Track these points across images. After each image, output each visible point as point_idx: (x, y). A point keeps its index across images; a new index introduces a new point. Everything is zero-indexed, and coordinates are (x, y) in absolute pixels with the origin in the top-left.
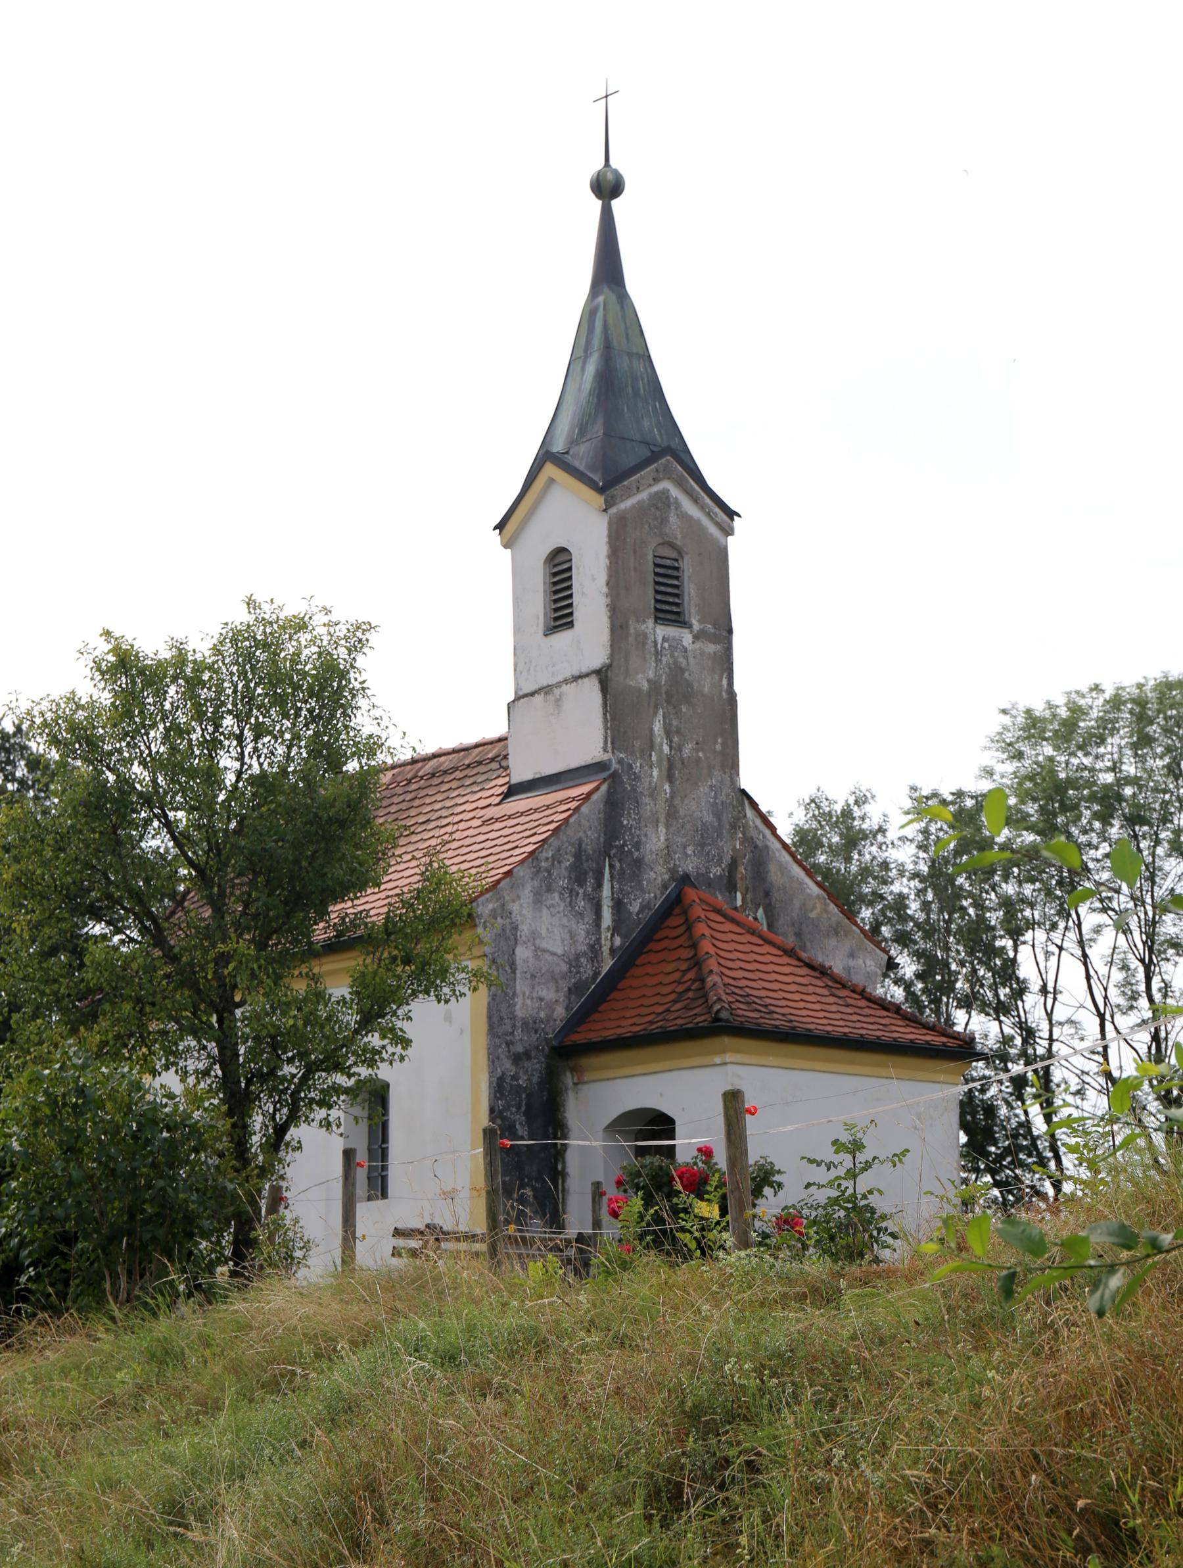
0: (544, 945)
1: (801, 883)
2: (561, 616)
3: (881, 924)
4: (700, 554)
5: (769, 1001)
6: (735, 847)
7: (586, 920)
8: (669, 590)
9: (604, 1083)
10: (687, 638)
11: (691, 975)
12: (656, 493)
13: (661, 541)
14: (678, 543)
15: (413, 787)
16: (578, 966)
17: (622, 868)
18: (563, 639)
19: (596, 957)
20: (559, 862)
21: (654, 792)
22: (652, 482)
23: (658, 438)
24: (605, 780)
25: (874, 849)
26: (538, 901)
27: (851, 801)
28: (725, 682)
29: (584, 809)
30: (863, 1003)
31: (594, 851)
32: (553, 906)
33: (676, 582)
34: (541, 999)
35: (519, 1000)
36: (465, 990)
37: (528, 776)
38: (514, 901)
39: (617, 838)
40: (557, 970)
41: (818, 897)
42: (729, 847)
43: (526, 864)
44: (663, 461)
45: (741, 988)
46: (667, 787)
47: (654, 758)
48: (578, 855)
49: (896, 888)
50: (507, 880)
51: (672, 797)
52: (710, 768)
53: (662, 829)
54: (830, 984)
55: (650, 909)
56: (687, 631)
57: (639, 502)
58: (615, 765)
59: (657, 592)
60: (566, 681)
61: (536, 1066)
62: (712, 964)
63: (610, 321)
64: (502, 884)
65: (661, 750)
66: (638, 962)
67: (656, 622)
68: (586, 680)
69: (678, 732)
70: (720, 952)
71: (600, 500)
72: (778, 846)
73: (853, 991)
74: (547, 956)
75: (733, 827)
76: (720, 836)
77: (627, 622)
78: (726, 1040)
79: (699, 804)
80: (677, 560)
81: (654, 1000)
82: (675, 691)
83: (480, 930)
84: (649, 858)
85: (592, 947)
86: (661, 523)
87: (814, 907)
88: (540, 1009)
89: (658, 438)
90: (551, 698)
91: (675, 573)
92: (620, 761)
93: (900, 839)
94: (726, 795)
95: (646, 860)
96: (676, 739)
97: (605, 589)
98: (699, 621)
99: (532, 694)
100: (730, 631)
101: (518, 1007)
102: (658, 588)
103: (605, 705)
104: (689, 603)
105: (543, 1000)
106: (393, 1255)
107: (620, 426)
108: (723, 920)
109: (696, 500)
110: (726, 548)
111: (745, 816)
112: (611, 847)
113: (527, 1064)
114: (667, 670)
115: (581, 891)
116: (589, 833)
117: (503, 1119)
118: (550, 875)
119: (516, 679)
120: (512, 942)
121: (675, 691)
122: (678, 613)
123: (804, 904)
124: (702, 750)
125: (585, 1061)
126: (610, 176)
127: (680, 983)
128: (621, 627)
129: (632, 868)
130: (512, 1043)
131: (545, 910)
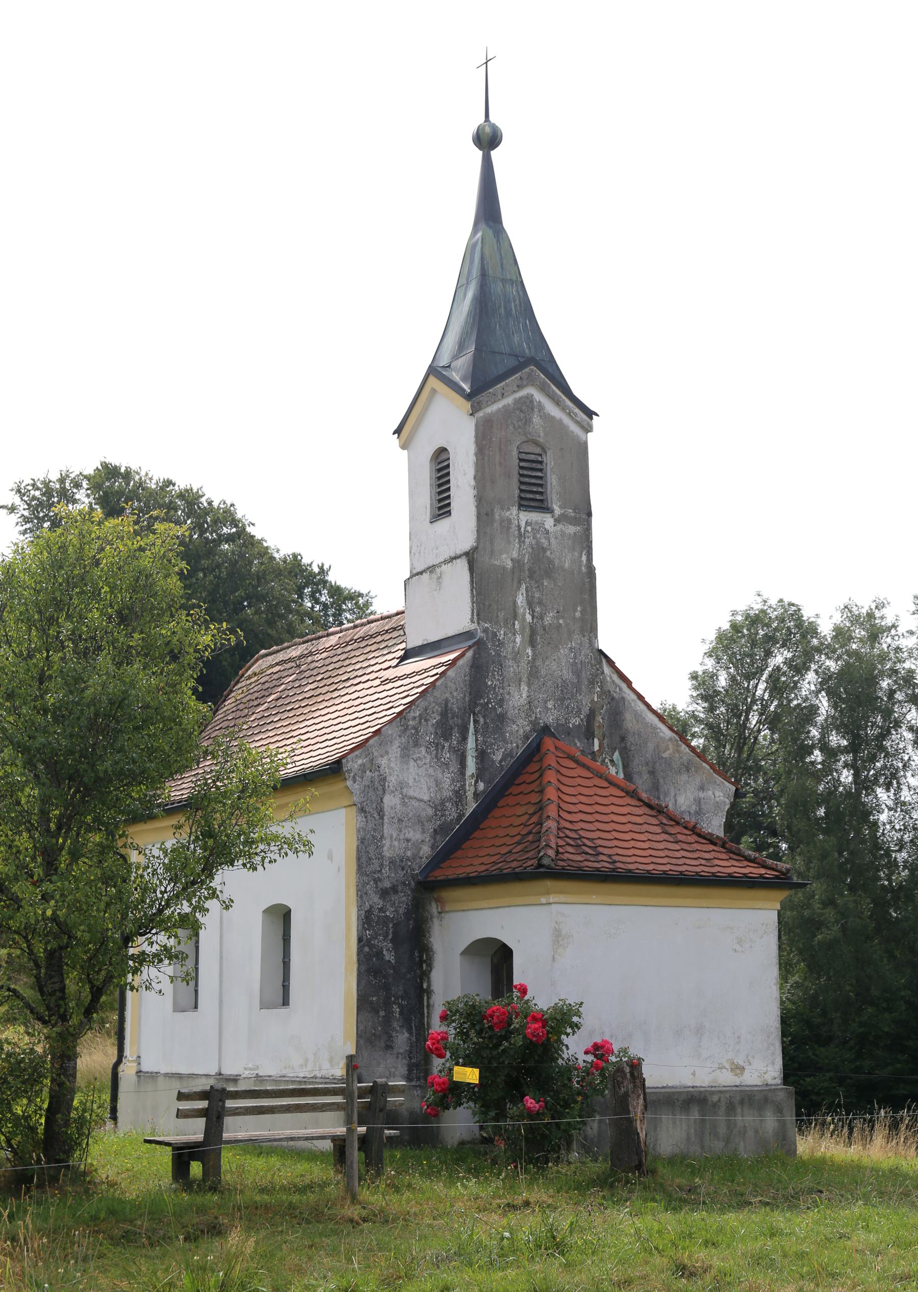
0: (411, 793)
1: (655, 728)
2: (442, 507)
3: (895, 692)
4: (562, 449)
5: (599, 842)
6: (593, 700)
7: (451, 769)
8: (533, 481)
9: (460, 913)
10: (549, 522)
11: (534, 819)
12: (521, 398)
13: (524, 438)
14: (541, 440)
15: (349, 648)
16: (443, 810)
17: (485, 723)
18: (444, 525)
19: (460, 801)
20: (426, 720)
21: (517, 656)
22: (516, 388)
23: (527, 351)
24: (470, 647)
25: (889, 640)
26: (405, 755)
27: (873, 607)
28: (584, 558)
29: (451, 673)
30: (694, 838)
31: (459, 709)
32: (420, 758)
33: (539, 474)
34: (408, 840)
35: (387, 843)
36: (277, 856)
37: (419, 643)
38: (382, 756)
39: (482, 697)
40: (424, 814)
41: (670, 739)
42: (585, 701)
43: (394, 723)
44: (527, 370)
45: (575, 831)
46: (529, 651)
47: (517, 626)
48: (444, 713)
49: (907, 665)
50: (376, 738)
51: (534, 659)
52: (570, 633)
53: (524, 688)
54: (665, 821)
55: (512, 757)
56: (549, 515)
57: (504, 406)
58: (480, 634)
59: (522, 483)
60: (445, 562)
61: (403, 900)
62: (552, 811)
63: (487, 252)
64: (371, 742)
65: (524, 619)
66: (499, 805)
67: (519, 509)
68: (459, 560)
69: (540, 603)
70: (561, 795)
71: (467, 405)
72: (634, 697)
73: (686, 828)
74: (413, 802)
75: (592, 683)
76: (579, 690)
77: (492, 510)
78: (549, 883)
79: (559, 664)
80: (541, 455)
81: (502, 841)
82: (538, 568)
83: (349, 783)
84: (511, 713)
85: (457, 793)
86: (525, 424)
87: (667, 749)
88: (407, 849)
89: (527, 351)
90: (434, 576)
91: (539, 466)
92: (485, 631)
93: (908, 632)
94: (585, 655)
95: (509, 714)
96: (538, 609)
97: (473, 483)
98: (560, 507)
99: (421, 573)
100: (590, 514)
101: (385, 849)
102: (523, 479)
103: (472, 581)
104: (551, 492)
105: (410, 840)
106: (177, 1117)
107: (498, 345)
108: (575, 766)
109: (557, 403)
110: (586, 443)
111: (603, 673)
112: (476, 704)
113: (394, 897)
114: (530, 550)
115: (447, 745)
116: (455, 694)
117: (371, 946)
118: (417, 732)
119: (411, 560)
120: (380, 792)
121: (538, 568)
122: (541, 501)
123: (658, 746)
124: (563, 617)
125: (447, 894)
126: (488, 130)
127: (526, 826)
128: (487, 514)
129: (498, 721)
130: (380, 880)
131: (412, 763)
